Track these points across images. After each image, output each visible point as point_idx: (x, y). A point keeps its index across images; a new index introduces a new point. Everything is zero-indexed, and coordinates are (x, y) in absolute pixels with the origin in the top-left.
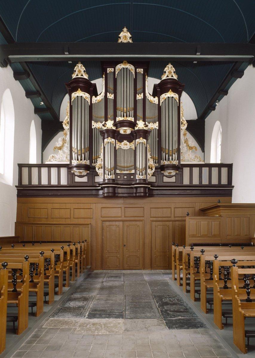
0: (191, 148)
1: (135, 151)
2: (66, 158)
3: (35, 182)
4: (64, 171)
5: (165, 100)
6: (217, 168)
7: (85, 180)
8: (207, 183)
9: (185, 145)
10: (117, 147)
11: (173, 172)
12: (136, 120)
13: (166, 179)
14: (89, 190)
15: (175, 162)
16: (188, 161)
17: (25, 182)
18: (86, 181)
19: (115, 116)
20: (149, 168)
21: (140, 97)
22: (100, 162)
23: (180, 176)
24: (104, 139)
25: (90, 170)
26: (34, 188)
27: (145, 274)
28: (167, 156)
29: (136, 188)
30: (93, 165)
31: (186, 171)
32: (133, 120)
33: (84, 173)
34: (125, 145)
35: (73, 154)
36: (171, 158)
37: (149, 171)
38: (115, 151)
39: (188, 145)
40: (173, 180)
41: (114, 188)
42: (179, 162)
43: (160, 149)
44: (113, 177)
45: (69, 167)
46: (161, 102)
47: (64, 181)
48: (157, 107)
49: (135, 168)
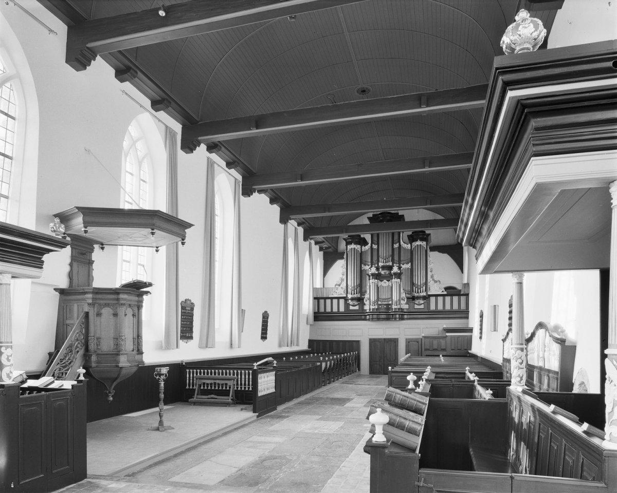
1: (392, 287)
4: (342, 302)
7: (357, 308)
8: (330, 311)
9: (431, 279)
11: (422, 302)
12: (393, 264)
13: (416, 307)
14: (360, 316)
15: (424, 294)
17: (322, 310)
19: (378, 261)
21: (396, 246)
22: (367, 296)
24: (369, 279)
25: (360, 300)
26: (11, 246)
30: (363, 297)
31: (433, 299)
33: (356, 303)
34: (385, 283)
35: (349, 289)
37: (402, 302)
39: (433, 280)
40: (422, 307)
43: (413, 284)
44: (376, 307)
45: (345, 299)
46: (413, 248)
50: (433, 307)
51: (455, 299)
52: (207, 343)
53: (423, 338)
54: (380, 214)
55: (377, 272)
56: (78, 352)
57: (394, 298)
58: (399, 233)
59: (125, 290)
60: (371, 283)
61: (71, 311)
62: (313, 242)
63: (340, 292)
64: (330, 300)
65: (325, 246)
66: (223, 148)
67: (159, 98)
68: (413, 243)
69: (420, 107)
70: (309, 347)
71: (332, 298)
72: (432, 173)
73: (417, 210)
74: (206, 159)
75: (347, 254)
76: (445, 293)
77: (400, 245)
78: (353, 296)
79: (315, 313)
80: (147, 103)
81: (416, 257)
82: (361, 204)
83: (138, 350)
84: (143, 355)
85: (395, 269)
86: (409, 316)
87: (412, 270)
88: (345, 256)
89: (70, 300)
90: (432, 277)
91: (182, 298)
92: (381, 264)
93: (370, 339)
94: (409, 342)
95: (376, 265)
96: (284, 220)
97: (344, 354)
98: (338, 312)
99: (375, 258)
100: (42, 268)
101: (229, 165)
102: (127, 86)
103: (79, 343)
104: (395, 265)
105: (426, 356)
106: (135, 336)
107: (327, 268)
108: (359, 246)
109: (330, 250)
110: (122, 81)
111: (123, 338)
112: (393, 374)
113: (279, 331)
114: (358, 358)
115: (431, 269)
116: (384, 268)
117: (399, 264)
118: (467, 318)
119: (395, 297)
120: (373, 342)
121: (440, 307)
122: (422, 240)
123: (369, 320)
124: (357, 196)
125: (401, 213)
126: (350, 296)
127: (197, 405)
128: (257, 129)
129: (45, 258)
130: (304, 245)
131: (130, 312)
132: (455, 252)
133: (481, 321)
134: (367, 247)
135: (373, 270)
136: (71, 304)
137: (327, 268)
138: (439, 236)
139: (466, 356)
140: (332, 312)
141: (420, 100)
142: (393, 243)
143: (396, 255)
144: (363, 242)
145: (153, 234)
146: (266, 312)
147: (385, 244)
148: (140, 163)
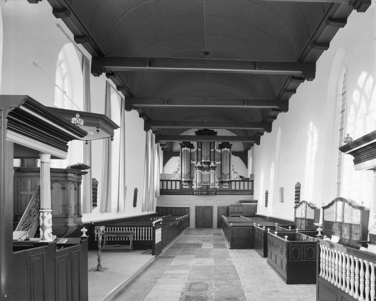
1: (210, 175)
4: (178, 183)
7: (187, 187)
8: (174, 188)
13: (224, 187)
14: (190, 192)
15: (228, 180)
19: (201, 159)
21: (212, 150)
22: (194, 180)
24: (196, 170)
25: (190, 182)
29: (210, 192)
30: (192, 180)
31: (233, 183)
32: (209, 161)
33: (187, 184)
34: (206, 173)
35: (183, 175)
37: (216, 184)
38: (202, 175)
40: (227, 187)
41: (216, 192)
43: (222, 174)
44: (200, 187)
45: (181, 181)
50: (233, 188)
51: (246, 183)
52: (106, 209)
53: (230, 206)
54: (202, 130)
55: (201, 166)
56: (35, 215)
57: (211, 182)
58: (214, 143)
59: (73, 170)
60: (197, 173)
61: (25, 184)
62: (159, 144)
63: (177, 177)
64: (170, 182)
65: (165, 147)
66: (117, 76)
67: (81, 34)
68: (222, 149)
69: (255, 69)
70: (157, 211)
71: (172, 181)
72: (170, 108)
73: (221, 129)
74: (105, 82)
75: (182, 153)
76: (241, 180)
77: (214, 150)
78: (185, 180)
79: (161, 190)
80: (72, 36)
81: (224, 158)
82: (190, 124)
83: (78, 214)
84: (82, 218)
85: (212, 164)
86: (219, 193)
87: (221, 165)
88: (180, 154)
89: (24, 176)
90: (233, 170)
91: (93, 177)
92: (203, 161)
93: (196, 207)
94: (219, 208)
95: (200, 161)
96: (146, 129)
97: (164, 216)
98: (176, 189)
99: (199, 157)
100: (67, 151)
101: (119, 88)
102: (60, 21)
103: (35, 209)
104: (211, 161)
105: (232, 216)
106: (76, 204)
107: (165, 162)
108: (189, 149)
109: (168, 150)
110: (57, 17)
111: (70, 205)
112: (234, 228)
113: (143, 202)
114: (188, 219)
115: (233, 165)
116: (205, 163)
117: (214, 161)
118: (252, 194)
119: (212, 181)
120: (197, 208)
121: (237, 188)
122: (228, 147)
123: (196, 195)
124: (188, 118)
125: (215, 130)
126: (183, 180)
127: (105, 252)
128: (150, 67)
129: (69, 144)
130: (155, 145)
131: (72, 186)
132: (244, 156)
133: (267, 197)
134: (195, 150)
135: (199, 164)
136: (26, 179)
137: (165, 162)
138: (237, 146)
139: (254, 217)
140: (171, 189)
141: (255, 65)
142: (210, 148)
143: (212, 156)
144: (191, 146)
145: (98, 131)
146: (136, 188)
147: (206, 153)
148: (64, 79)
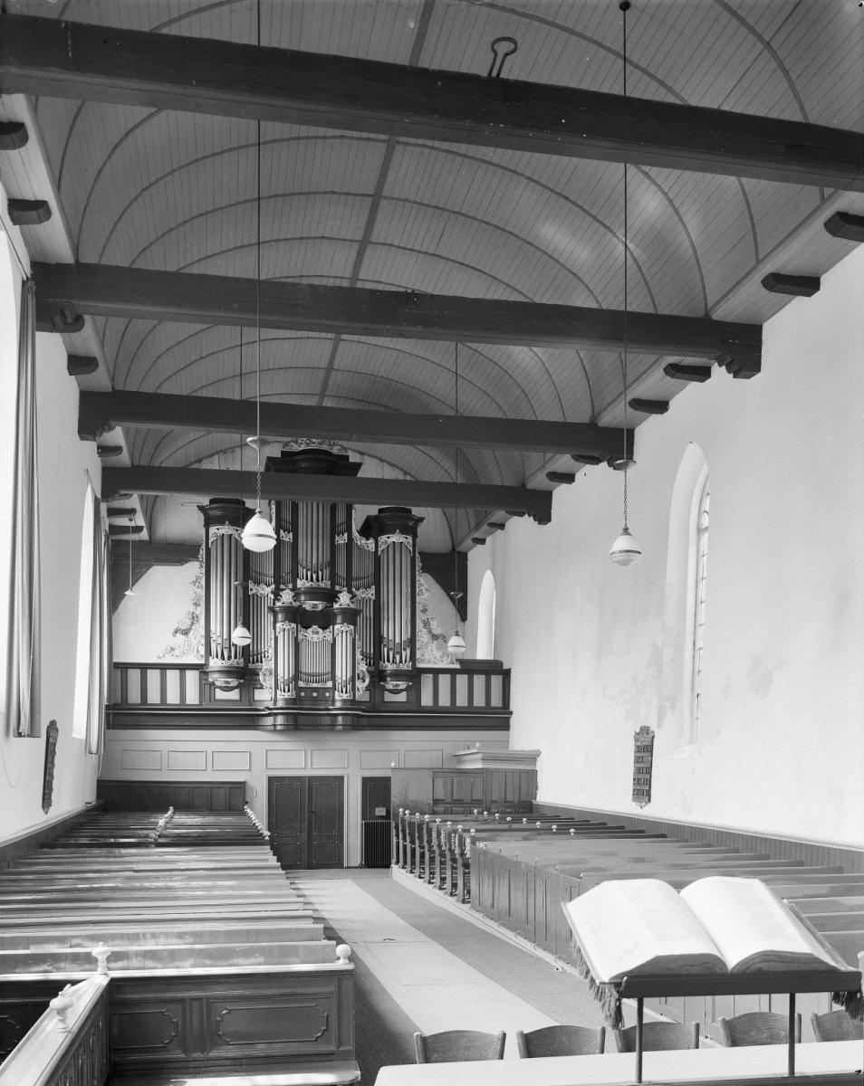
0: (435, 637)
2: (198, 651)
3: (154, 697)
4: (192, 676)
5: (388, 547)
6: (483, 676)
10: (300, 637)
11: (403, 685)
13: (389, 697)
15: (407, 666)
16: (429, 662)
18: (237, 698)
20: (359, 678)
21: (341, 540)
23: (415, 690)
27: (302, 460)
28: (391, 653)
31: (427, 680)
33: (234, 682)
36: (398, 657)
37: (359, 684)
40: (402, 697)
42: (414, 664)
45: (201, 669)
47: (192, 698)
48: (372, 557)
49: (333, 678)
